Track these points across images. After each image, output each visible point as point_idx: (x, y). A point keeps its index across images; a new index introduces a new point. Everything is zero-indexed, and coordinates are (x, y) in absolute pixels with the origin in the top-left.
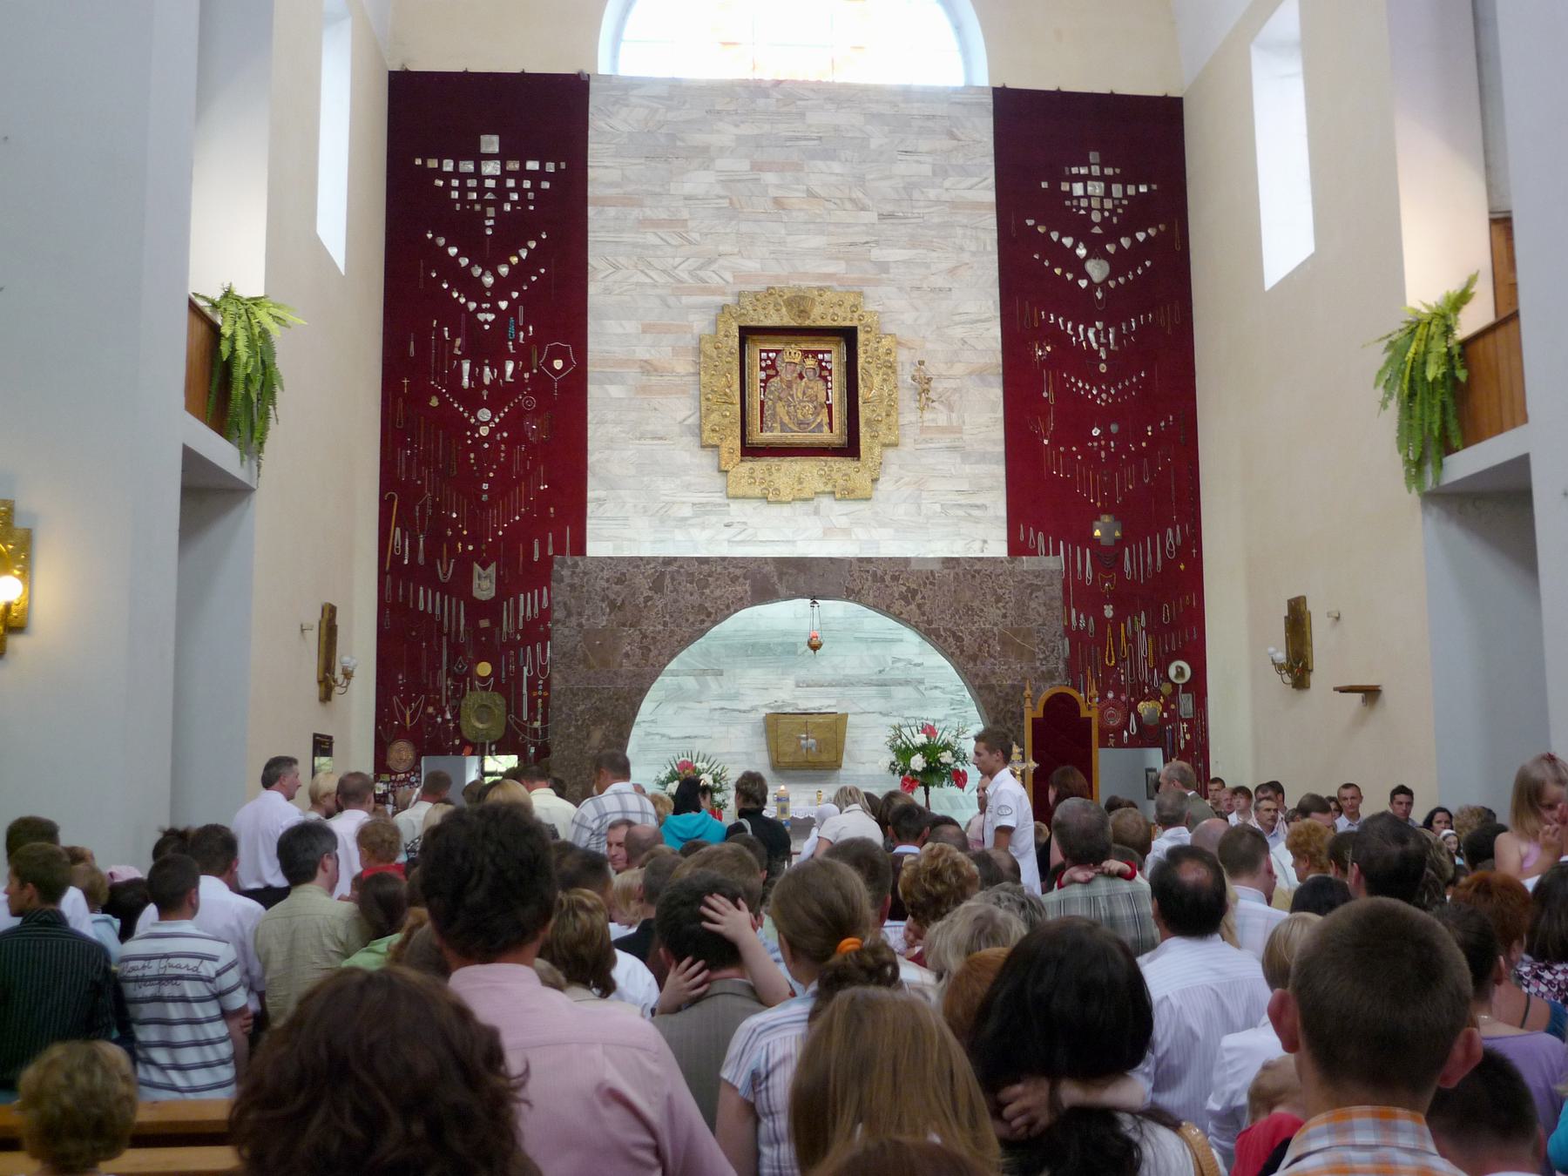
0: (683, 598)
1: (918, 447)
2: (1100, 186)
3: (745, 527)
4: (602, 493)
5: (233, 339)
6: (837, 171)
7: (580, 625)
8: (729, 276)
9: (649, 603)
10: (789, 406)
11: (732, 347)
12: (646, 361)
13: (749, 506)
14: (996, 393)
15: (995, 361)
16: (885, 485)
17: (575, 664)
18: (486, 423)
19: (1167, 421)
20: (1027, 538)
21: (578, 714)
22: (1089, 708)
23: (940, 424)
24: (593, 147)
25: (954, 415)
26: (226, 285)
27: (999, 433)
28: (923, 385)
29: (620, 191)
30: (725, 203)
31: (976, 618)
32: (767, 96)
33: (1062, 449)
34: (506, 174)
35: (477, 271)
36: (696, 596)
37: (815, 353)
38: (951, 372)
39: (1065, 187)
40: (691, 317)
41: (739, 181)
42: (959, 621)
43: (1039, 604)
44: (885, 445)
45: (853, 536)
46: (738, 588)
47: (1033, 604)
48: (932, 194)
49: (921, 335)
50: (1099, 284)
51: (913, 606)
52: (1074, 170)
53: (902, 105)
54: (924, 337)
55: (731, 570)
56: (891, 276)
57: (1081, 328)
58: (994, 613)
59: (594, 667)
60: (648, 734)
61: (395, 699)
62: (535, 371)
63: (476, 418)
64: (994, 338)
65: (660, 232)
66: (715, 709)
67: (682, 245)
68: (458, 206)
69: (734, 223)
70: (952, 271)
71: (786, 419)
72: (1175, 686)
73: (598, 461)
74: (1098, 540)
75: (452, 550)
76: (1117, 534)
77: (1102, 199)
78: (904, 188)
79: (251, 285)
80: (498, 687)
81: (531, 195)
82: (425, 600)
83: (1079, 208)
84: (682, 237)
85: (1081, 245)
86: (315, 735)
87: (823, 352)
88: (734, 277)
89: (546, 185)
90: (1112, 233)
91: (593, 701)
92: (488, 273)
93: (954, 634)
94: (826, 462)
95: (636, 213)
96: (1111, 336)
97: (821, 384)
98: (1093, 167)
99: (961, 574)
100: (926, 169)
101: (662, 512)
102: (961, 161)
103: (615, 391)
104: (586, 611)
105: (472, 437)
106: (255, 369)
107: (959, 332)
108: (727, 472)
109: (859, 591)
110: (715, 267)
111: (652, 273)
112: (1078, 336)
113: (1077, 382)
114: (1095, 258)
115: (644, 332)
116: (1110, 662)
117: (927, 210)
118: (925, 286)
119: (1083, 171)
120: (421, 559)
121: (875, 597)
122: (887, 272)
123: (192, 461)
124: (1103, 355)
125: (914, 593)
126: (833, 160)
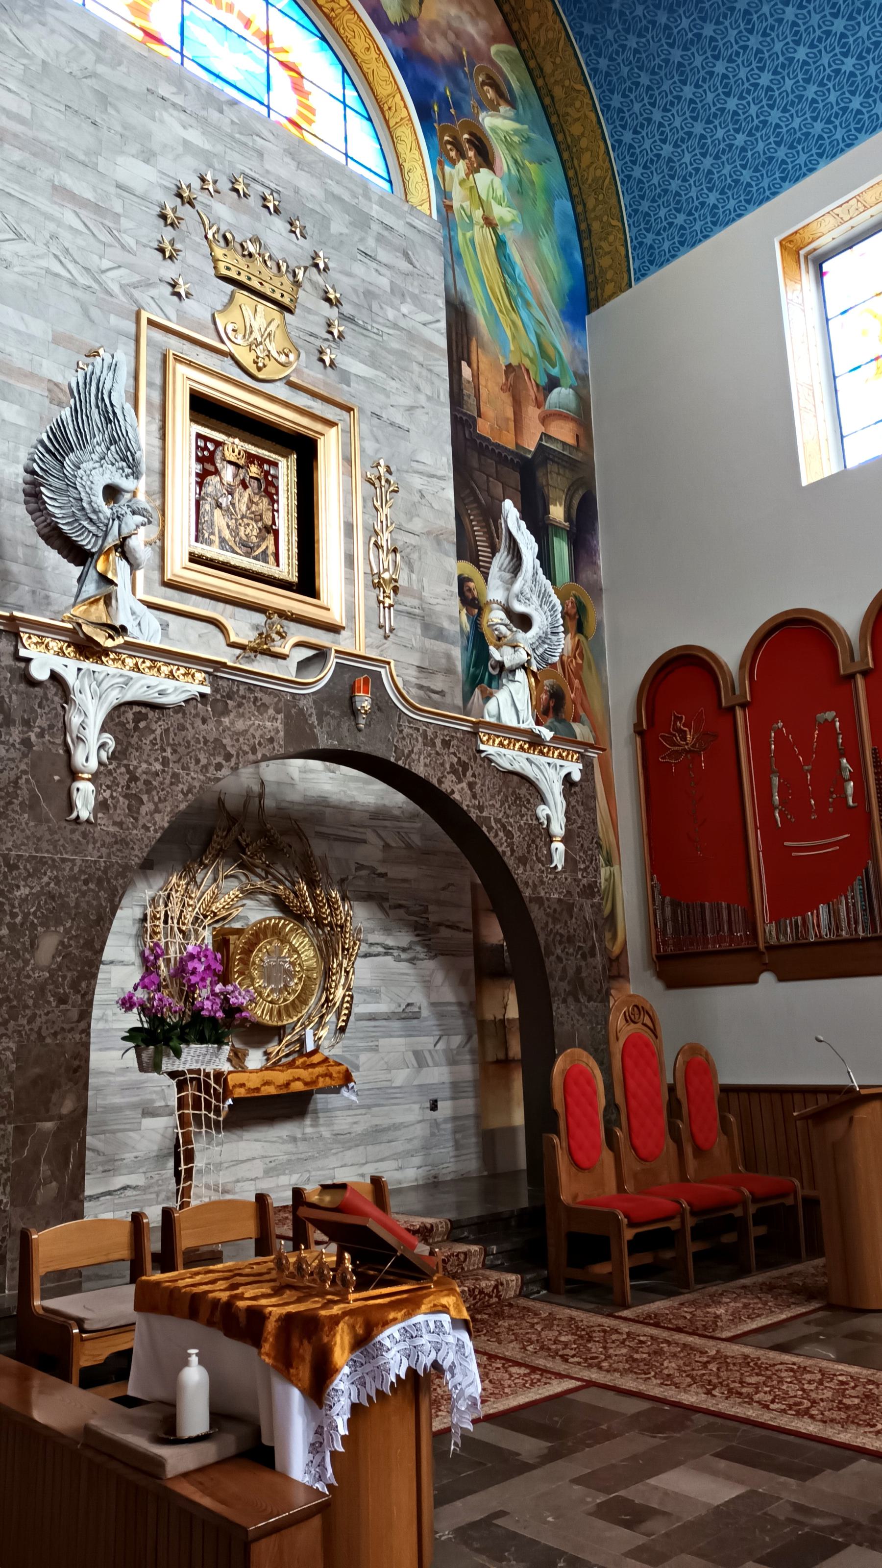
0: (192, 724)
7: (26, 742)
9: (142, 725)
12: (56, 384)
17: (14, 811)
21: (16, 903)
25: (414, 576)
29: (30, 133)
36: (211, 725)
37: (262, 461)
42: (508, 811)
43: (577, 802)
46: (268, 724)
48: (391, 314)
51: (464, 785)
59: (48, 820)
65: (83, 213)
67: (111, 246)
70: (411, 409)
91: (45, 879)
104: (39, 720)
109: (409, 755)
110: (154, 292)
111: (70, 266)
121: (426, 765)
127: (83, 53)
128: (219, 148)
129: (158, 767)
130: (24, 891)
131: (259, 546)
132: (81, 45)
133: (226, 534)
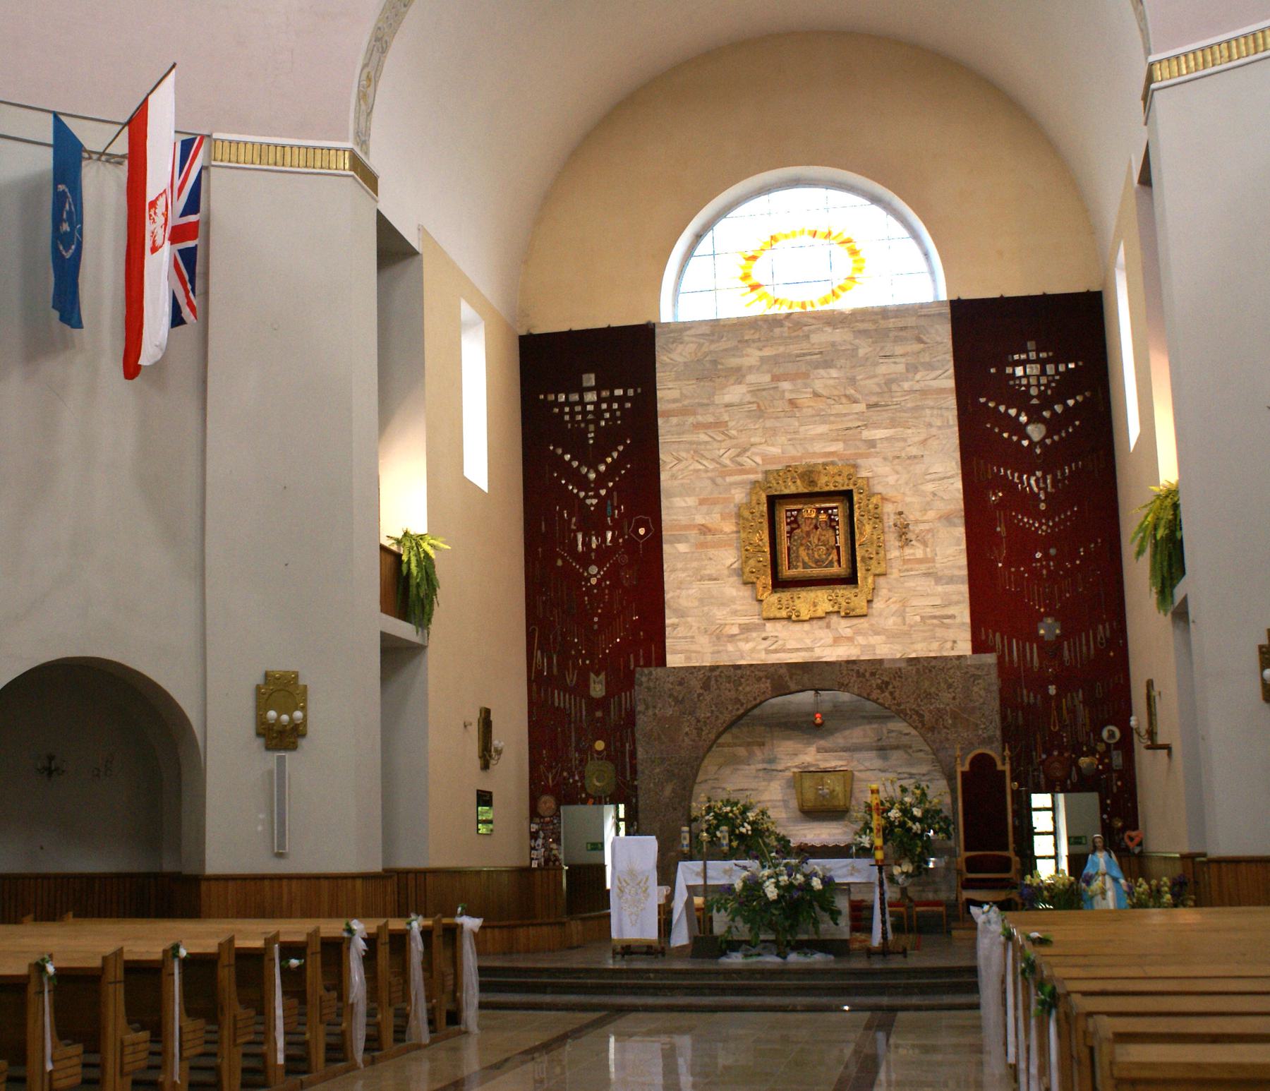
1: (902, 574)
2: (1037, 368)
3: (775, 639)
4: (674, 620)
5: (409, 562)
6: (835, 376)
8: (758, 460)
9: (701, 698)
10: (808, 549)
11: (762, 511)
12: (702, 525)
13: (779, 625)
14: (960, 531)
15: (958, 507)
16: (878, 605)
18: (595, 576)
19: (1096, 543)
20: (987, 636)
22: (1004, 764)
23: (918, 557)
24: (659, 375)
25: (928, 550)
26: (405, 529)
27: (963, 560)
28: (903, 532)
29: (680, 405)
30: (754, 407)
31: (933, 700)
32: (782, 326)
33: (1013, 569)
34: (600, 400)
35: (584, 470)
36: (733, 692)
37: (826, 509)
38: (925, 518)
39: (1009, 370)
40: (733, 491)
41: (764, 390)
43: (980, 689)
44: (875, 575)
45: (856, 643)
46: (762, 686)
47: (975, 689)
48: (906, 386)
49: (902, 491)
50: (1038, 443)
51: (887, 694)
52: (1016, 357)
53: (882, 322)
54: (904, 493)
55: (757, 673)
56: (878, 450)
57: (1025, 477)
58: (946, 696)
60: (714, 788)
61: (541, 766)
62: (626, 537)
63: (588, 572)
64: (958, 490)
65: (710, 432)
66: (760, 770)
67: (724, 440)
68: (569, 426)
69: (761, 421)
70: (924, 442)
71: (806, 559)
72: (1108, 745)
73: (672, 598)
74: (1042, 637)
75: (575, 666)
76: (1058, 631)
77: (1038, 377)
78: (885, 383)
79: (419, 526)
80: (609, 758)
81: (618, 413)
82: (559, 699)
83: (1021, 386)
84: (723, 433)
85: (1023, 414)
86: (478, 791)
87: (832, 508)
88: (763, 460)
89: (628, 405)
90: (1047, 402)
92: (592, 471)
93: (917, 713)
94: (833, 590)
95: (691, 420)
96: (1048, 481)
97: (831, 532)
98: (1031, 354)
99: (921, 670)
100: (901, 368)
101: (718, 632)
102: (927, 359)
103: (682, 547)
105: (585, 586)
106: (422, 579)
107: (930, 487)
108: (762, 601)
110: (748, 454)
111: (705, 462)
112: (1022, 483)
113: (1022, 518)
114: (1034, 423)
115: (700, 504)
116: (1055, 726)
117: (904, 398)
118: (903, 455)
119: (1023, 356)
120: (555, 670)
121: (859, 688)
122: (874, 446)
123: (385, 637)
124: (1042, 496)
125: (887, 684)
126: (830, 367)
127: (703, 344)
128: (782, 349)
129: (709, 714)
130: (658, 770)
131: (827, 559)
132: (702, 341)
133: (806, 559)
